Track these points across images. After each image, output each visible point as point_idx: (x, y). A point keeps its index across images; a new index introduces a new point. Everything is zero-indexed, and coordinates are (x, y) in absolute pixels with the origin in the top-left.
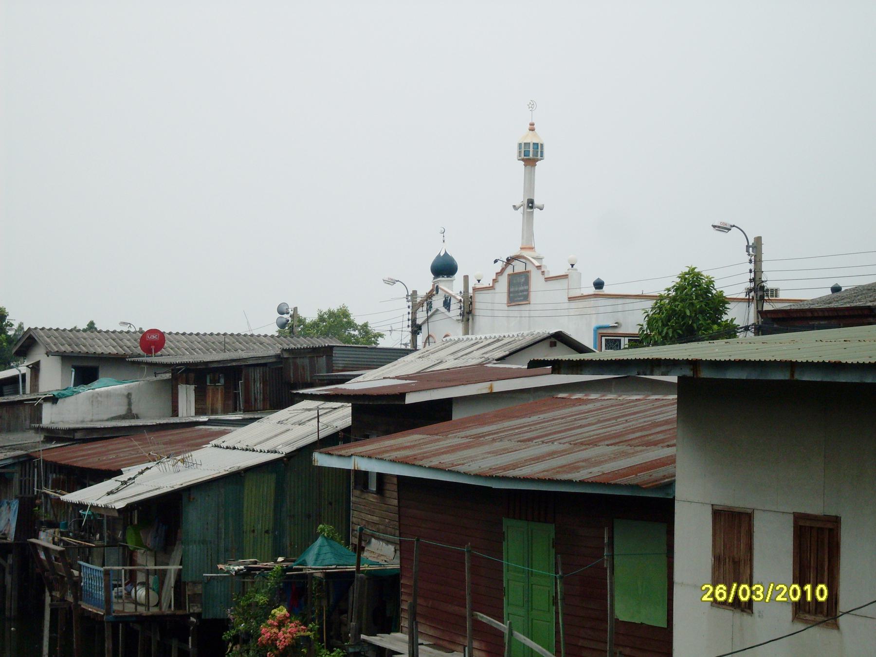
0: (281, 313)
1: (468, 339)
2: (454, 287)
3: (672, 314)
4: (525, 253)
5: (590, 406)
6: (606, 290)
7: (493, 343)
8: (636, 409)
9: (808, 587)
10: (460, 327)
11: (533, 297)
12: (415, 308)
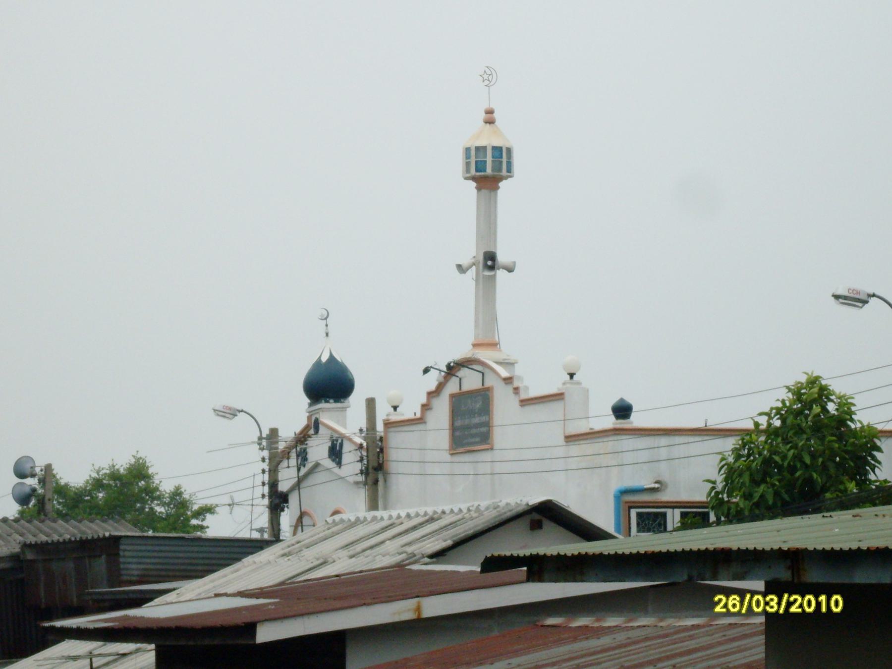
0: (21, 475)
1: (374, 519)
2: (348, 420)
3: (762, 475)
4: (484, 355)
5: (606, 641)
6: (636, 420)
7: (421, 525)
8: (692, 644)
9: (823, 598)
10: (361, 496)
11: (499, 436)
12: (275, 461)
